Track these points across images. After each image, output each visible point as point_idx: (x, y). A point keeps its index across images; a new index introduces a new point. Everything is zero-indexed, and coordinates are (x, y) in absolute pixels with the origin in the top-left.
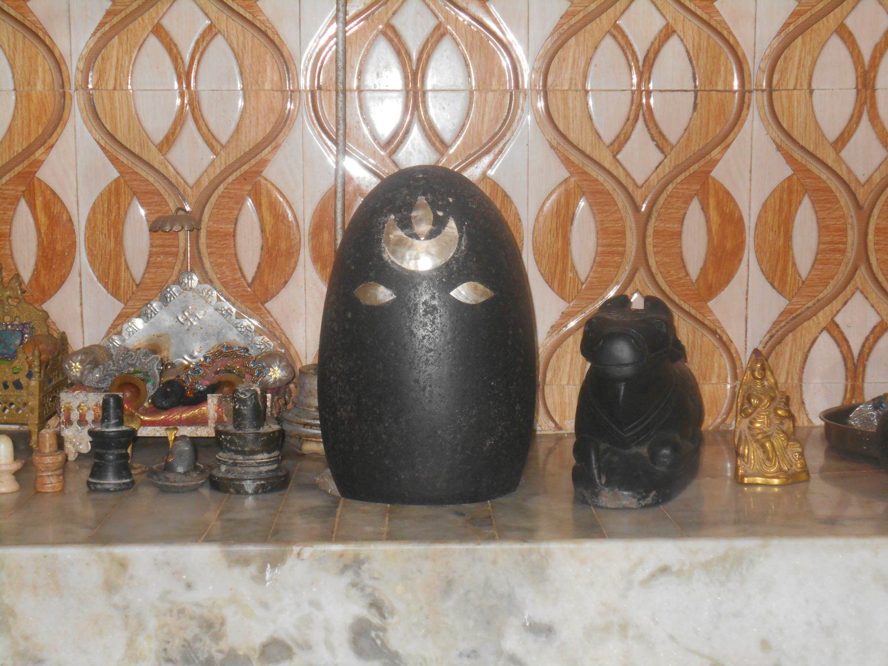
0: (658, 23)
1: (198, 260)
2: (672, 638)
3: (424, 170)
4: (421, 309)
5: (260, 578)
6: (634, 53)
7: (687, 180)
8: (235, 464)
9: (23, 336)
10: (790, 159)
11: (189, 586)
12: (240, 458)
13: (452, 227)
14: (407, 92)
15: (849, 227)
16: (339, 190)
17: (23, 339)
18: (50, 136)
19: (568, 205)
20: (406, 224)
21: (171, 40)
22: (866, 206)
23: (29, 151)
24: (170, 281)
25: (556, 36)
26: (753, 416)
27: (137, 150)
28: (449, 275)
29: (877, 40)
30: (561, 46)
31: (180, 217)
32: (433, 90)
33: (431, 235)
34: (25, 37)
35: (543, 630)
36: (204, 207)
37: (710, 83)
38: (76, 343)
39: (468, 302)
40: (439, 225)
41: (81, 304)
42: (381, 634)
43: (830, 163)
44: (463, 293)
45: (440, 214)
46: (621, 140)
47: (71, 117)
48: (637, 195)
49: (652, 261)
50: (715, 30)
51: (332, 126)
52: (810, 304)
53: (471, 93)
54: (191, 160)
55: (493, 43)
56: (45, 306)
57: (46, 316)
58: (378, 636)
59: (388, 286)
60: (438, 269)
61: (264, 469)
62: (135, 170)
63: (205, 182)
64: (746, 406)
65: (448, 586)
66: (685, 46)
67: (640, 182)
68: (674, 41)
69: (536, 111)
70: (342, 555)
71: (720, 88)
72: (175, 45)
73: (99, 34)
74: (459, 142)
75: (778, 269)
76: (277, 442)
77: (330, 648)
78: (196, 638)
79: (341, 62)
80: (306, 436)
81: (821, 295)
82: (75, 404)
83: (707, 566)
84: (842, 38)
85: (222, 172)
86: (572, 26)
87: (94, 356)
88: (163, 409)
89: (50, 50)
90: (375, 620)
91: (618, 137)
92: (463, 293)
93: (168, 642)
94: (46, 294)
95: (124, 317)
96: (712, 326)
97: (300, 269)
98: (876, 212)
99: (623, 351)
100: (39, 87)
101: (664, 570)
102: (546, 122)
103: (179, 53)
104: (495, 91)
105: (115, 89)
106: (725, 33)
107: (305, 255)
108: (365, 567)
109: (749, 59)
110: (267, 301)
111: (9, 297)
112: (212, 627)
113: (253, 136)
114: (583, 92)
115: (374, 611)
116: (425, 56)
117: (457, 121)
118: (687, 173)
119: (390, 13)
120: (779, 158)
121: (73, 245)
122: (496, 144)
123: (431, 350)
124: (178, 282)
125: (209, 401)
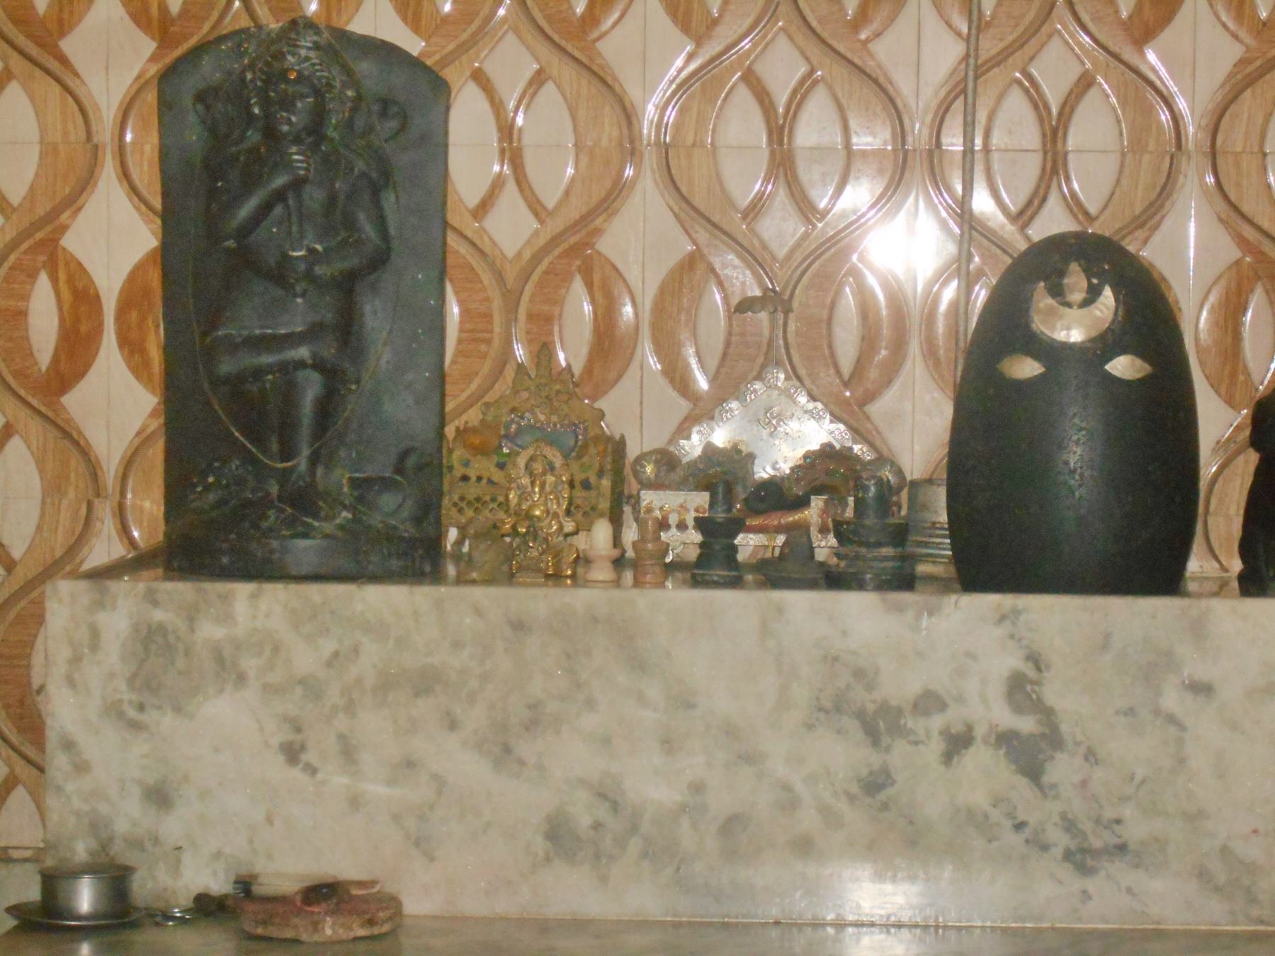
12: (863, 550)
13: (1108, 294)
14: (1045, 153)
17: (576, 442)
19: (1239, 295)
20: (1057, 292)
24: (750, 378)
25: (1228, 87)
28: (1106, 345)
30: (1235, 98)
34: (590, 82)
35: (1201, 689)
40: (1093, 294)
42: (1037, 688)
44: (1123, 366)
45: (1095, 281)
53: (1123, 155)
55: (1151, 95)
56: (601, 404)
58: (1035, 692)
59: (1036, 357)
60: (1092, 340)
61: (890, 564)
72: (768, 94)
78: (848, 687)
82: (656, 504)
85: (12, 240)
88: (758, 513)
92: (1123, 366)
97: (908, 364)
100: (605, 143)
103: (501, 102)
104: (1151, 152)
105: (694, 145)
108: (1023, 618)
111: (558, 392)
114: (1260, 155)
115: (1030, 664)
124: (759, 377)
125: (813, 504)
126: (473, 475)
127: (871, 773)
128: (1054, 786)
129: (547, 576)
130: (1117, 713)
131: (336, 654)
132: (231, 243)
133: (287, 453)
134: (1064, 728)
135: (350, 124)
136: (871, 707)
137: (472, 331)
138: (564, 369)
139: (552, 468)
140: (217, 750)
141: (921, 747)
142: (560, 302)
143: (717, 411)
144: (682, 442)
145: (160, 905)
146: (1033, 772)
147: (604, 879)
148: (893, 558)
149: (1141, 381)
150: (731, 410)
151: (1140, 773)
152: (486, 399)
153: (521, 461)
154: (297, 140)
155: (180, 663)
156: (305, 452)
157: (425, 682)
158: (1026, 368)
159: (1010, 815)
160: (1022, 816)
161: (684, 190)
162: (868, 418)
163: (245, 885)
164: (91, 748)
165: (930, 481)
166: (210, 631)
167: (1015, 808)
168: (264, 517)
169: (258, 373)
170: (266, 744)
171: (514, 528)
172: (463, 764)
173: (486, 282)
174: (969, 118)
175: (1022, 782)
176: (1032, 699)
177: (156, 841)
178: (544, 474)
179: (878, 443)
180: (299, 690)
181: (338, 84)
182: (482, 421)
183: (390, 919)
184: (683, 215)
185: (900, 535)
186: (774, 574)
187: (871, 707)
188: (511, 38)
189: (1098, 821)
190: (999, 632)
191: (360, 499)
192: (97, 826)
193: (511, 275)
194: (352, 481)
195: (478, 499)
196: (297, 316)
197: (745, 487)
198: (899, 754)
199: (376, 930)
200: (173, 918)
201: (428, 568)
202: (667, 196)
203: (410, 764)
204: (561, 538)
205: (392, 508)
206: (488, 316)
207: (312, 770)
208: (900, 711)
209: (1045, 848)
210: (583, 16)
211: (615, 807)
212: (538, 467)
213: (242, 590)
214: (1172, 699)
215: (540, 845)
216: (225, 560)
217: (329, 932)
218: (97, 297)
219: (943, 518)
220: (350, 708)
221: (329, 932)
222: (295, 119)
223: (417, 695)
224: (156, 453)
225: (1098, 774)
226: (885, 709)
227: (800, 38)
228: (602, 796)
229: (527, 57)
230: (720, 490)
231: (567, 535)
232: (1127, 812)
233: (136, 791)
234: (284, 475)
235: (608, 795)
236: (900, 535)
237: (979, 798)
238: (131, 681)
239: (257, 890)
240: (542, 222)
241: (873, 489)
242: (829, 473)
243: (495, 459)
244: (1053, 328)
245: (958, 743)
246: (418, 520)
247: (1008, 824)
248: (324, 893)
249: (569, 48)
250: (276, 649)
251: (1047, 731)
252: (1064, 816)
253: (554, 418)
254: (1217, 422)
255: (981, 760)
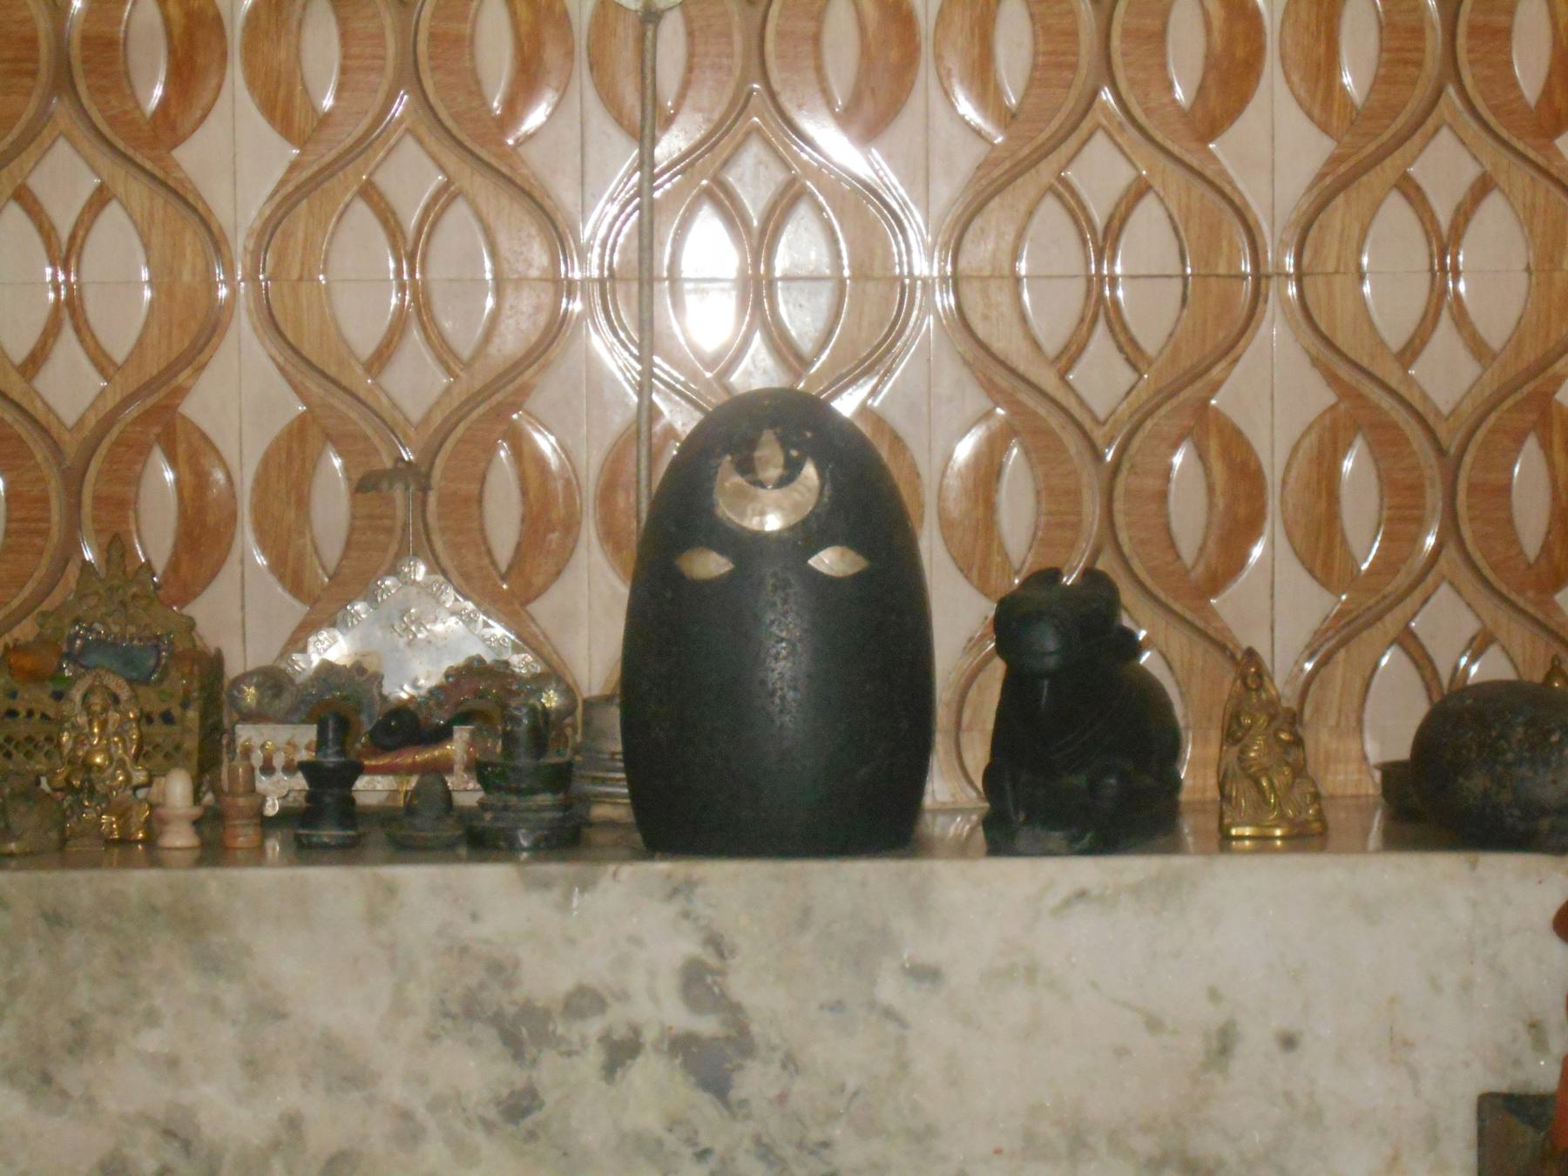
0: (1122, 176)
1: (423, 537)
2: (1094, 985)
4: (770, 581)
5: (564, 906)
6: (1089, 220)
7: (1517, 407)
8: (506, 808)
9: (159, 653)
10: (1332, 379)
12: (513, 800)
13: (810, 471)
15: (1427, 483)
16: (644, 428)
17: (159, 659)
18: (201, 351)
20: (746, 467)
21: (387, 204)
22: (1453, 450)
23: (172, 370)
26: (1246, 741)
27: (332, 371)
28: (809, 534)
29: (1459, 197)
31: (402, 471)
32: (787, 278)
33: (782, 482)
35: (926, 974)
36: (436, 454)
37: (1207, 264)
38: (234, 667)
39: (832, 573)
40: (791, 472)
41: (243, 607)
43: (1393, 382)
44: (829, 561)
45: (794, 453)
47: (234, 324)
48: (1098, 435)
49: (1123, 537)
50: (1211, 184)
52: (1371, 602)
54: (415, 385)
57: (191, 625)
58: (715, 982)
59: (722, 551)
60: (792, 529)
61: (548, 815)
62: (331, 397)
63: (437, 419)
64: (1235, 727)
65: (805, 918)
66: (1167, 209)
68: (1149, 205)
69: (1284, 300)
71: (1222, 270)
72: (394, 213)
73: (278, 198)
74: (824, 357)
75: (1321, 549)
77: (655, 999)
78: (482, 986)
79: (646, 238)
80: (596, 796)
81: (1389, 589)
82: (257, 741)
83: (1137, 890)
84: (1406, 196)
86: (994, 181)
88: (386, 749)
89: (205, 221)
90: (712, 960)
91: (1066, 348)
92: (829, 561)
93: (446, 991)
94: (189, 593)
96: (1219, 638)
98: (1468, 459)
99: (1048, 641)
100: (186, 277)
101: (1082, 895)
102: (1299, 315)
104: (879, 279)
105: (300, 279)
106: (1228, 189)
107: (589, 532)
108: (700, 890)
109: (1265, 227)
110: (528, 601)
111: (134, 596)
112: (502, 970)
115: (710, 949)
116: (771, 227)
117: (821, 324)
118: (1518, 396)
119: (718, 164)
120: (1313, 379)
121: (233, 516)
122: (879, 360)
123: (782, 640)
124: (393, 571)
125: (456, 736)
127: (512, 1094)
128: (743, 1103)
129: (110, 843)
130: (822, 1007)
134: (755, 1028)
136: (511, 1010)
137: (24, 520)
138: (142, 566)
139: (116, 700)
141: (575, 1059)
142: (136, 481)
143: (339, 615)
144: (295, 657)
146: (717, 1084)
148: (553, 807)
149: (857, 577)
150: (358, 613)
151: (852, 1083)
152: (44, 607)
153: (77, 694)
158: (710, 565)
159: (691, 1141)
160: (704, 1141)
161: (290, 335)
162: (533, 619)
165: (607, 699)
167: (696, 1132)
171: (68, 780)
173: (39, 458)
174: (646, 241)
175: (705, 1102)
176: (713, 993)
178: (105, 710)
179: (547, 650)
182: (39, 635)
184: (289, 368)
185: (560, 778)
187: (511, 1010)
188: (410, 145)
190: (671, 910)
193: (71, 446)
195: (29, 739)
197: (371, 717)
198: (548, 1071)
202: (268, 343)
204: (129, 792)
208: (547, 1014)
210: (155, 113)
211: (186, 1146)
212: (97, 702)
214: (890, 990)
219: (618, 747)
225: (799, 1086)
226: (528, 1010)
228: (169, 1133)
230: (331, 724)
231: (136, 788)
232: (837, 1132)
237: (649, 1120)
240: (107, 378)
241: (525, 721)
242: (480, 695)
243: (51, 687)
244: (742, 514)
245: (621, 1052)
247: (688, 1152)
249: (139, 159)
251: (733, 1033)
252: (757, 1140)
253: (132, 629)
254: (958, 618)
255: (650, 1075)
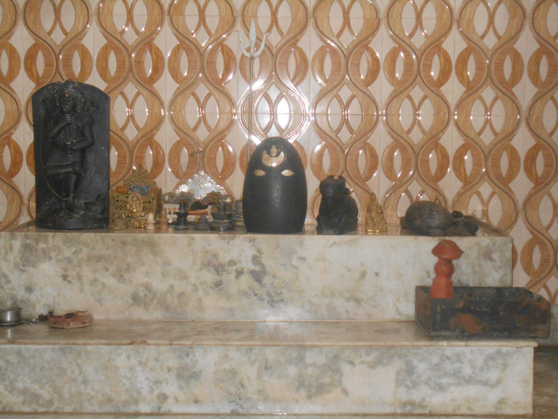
3: (275, 138)
5: (228, 243)
6: (343, 103)
11: (210, 245)
12: (220, 221)
13: (282, 154)
20: (269, 153)
28: (282, 167)
35: (303, 259)
38: (164, 191)
40: (278, 154)
46: (409, 131)
51: (247, 125)
54: (202, 134)
56: (155, 180)
57: (155, 183)
59: (263, 170)
60: (278, 166)
67: (344, 143)
68: (355, 99)
70: (250, 237)
76: (229, 217)
77: (246, 262)
82: (168, 207)
87: (171, 195)
95: (179, 184)
101: (335, 243)
107: (238, 165)
109: (379, 105)
112: (215, 256)
113: (222, 126)
118: (3, 137)
124: (197, 173)
126: (120, 200)
128: (264, 284)
129: (137, 228)
131: (76, 251)
132: (51, 140)
133: (67, 196)
134: (267, 269)
135: (83, 108)
136: (217, 264)
139: (139, 198)
140: (44, 277)
145: (30, 318)
147: (147, 310)
148: (228, 223)
151: (287, 280)
154: (68, 113)
155: (34, 254)
156: (72, 195)
157: (99, 259)
158: (261, 173)
160: (256, 292)
163: (51, 313)
164: (11, 277)
166: (42, 246)
168: (61, 213)
169: (58, 175)
170: (57, 275)
172: (111, 281)
175: (256, 284)
177: (29, 301)
180: (66, 261)
181: (79, 97)
183: (89, 322)
186: (197, 227)
187: (217, 264)
189: (276, 293)
190: (250, 244)
191: (86, 208)
192: (13, 297)
194: (85, 203)
196: (72, 158)
198: (224, 277)
199: (85, 325)
200: (33, 322)
201: (105, 226)
203: (96, 280)
205: (97, 209)
206: (125, 157)
207: (70, 282)
209: (262, 300)
211: (150, 291)
213: (50, 234)
214: (295, 262)
215: (130, 301)
216: (50, 225)
217: (72, 326)
218: (21, 152)
220: (80, 265)
221: (72, 326)
222: (67, 107)
223: (97, 262)
224: (34, 193)
227: (207, 84)
228: (146, 288)
229: (134, 88)
232: (284, 291)
233: (23, 288)
234: (66, 201)
235: (148, 287)
236: (229, 217)
238: (21, 259)
239: (54, 314)
245: (239, 273)
246: (102, 213)
247: (253, 294)
248: (70, 316)
250: (60, 250)
252: (267, 292)
254: (313, 185)
255: (246, 279)
